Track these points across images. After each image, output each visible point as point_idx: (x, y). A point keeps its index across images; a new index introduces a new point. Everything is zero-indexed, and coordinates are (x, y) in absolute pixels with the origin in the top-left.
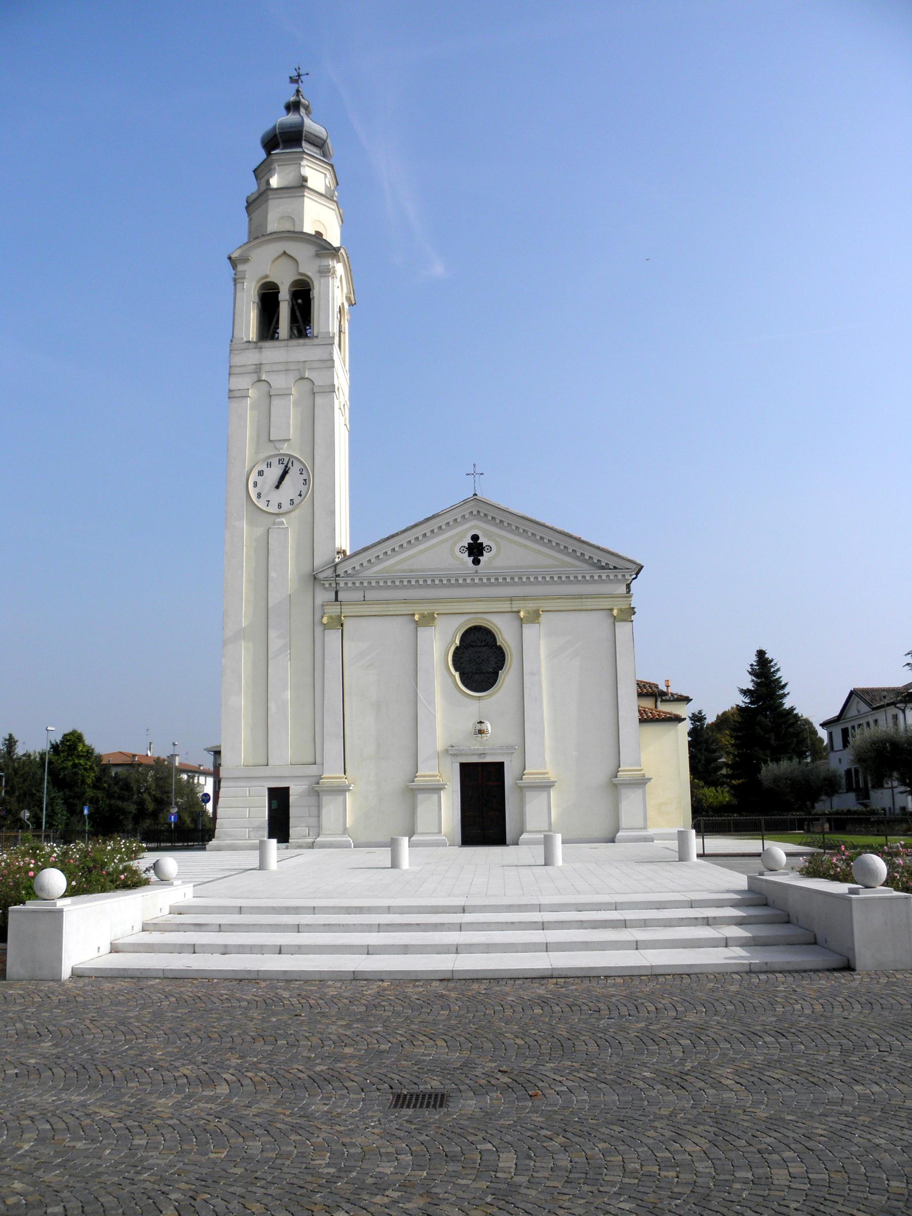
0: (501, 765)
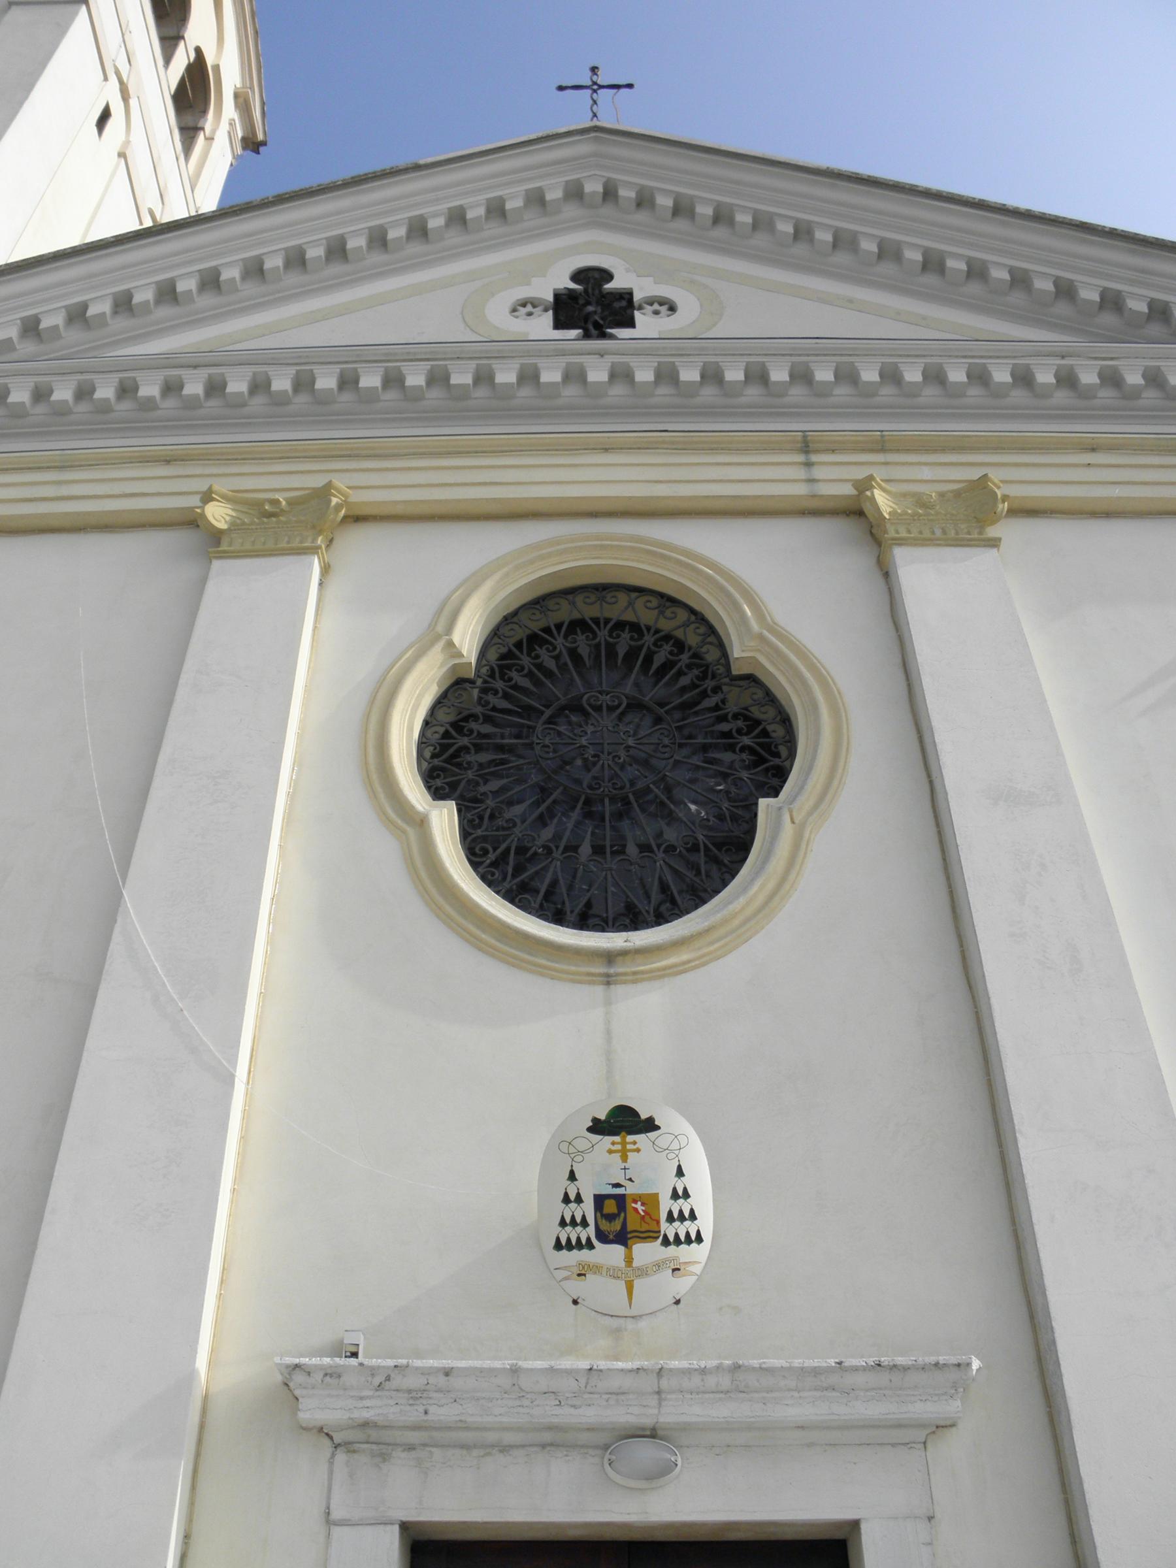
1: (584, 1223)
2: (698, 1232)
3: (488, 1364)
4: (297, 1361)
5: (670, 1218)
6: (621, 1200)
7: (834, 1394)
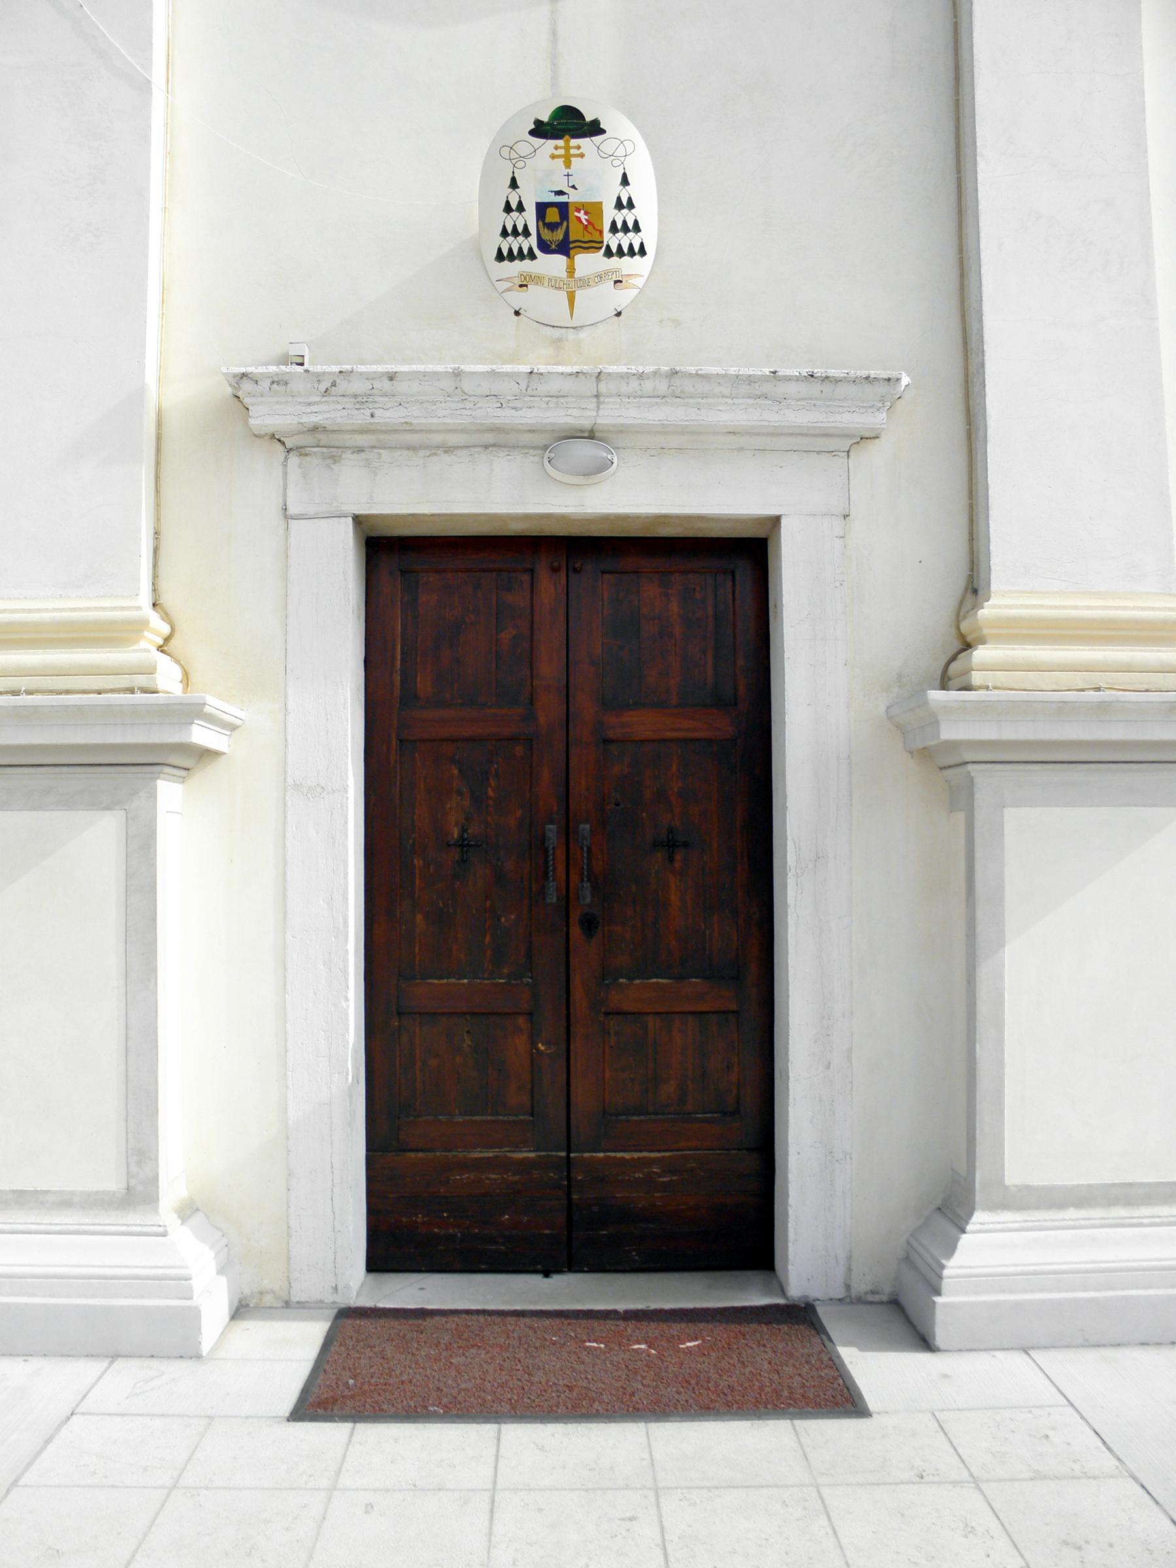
0: (742, 559)
1: (526, 233)
2: (642, 245)
3: (430, 368)
4: (243, 370)
5: (614, 229)
6: (563, 208)
7: (767, 402)
